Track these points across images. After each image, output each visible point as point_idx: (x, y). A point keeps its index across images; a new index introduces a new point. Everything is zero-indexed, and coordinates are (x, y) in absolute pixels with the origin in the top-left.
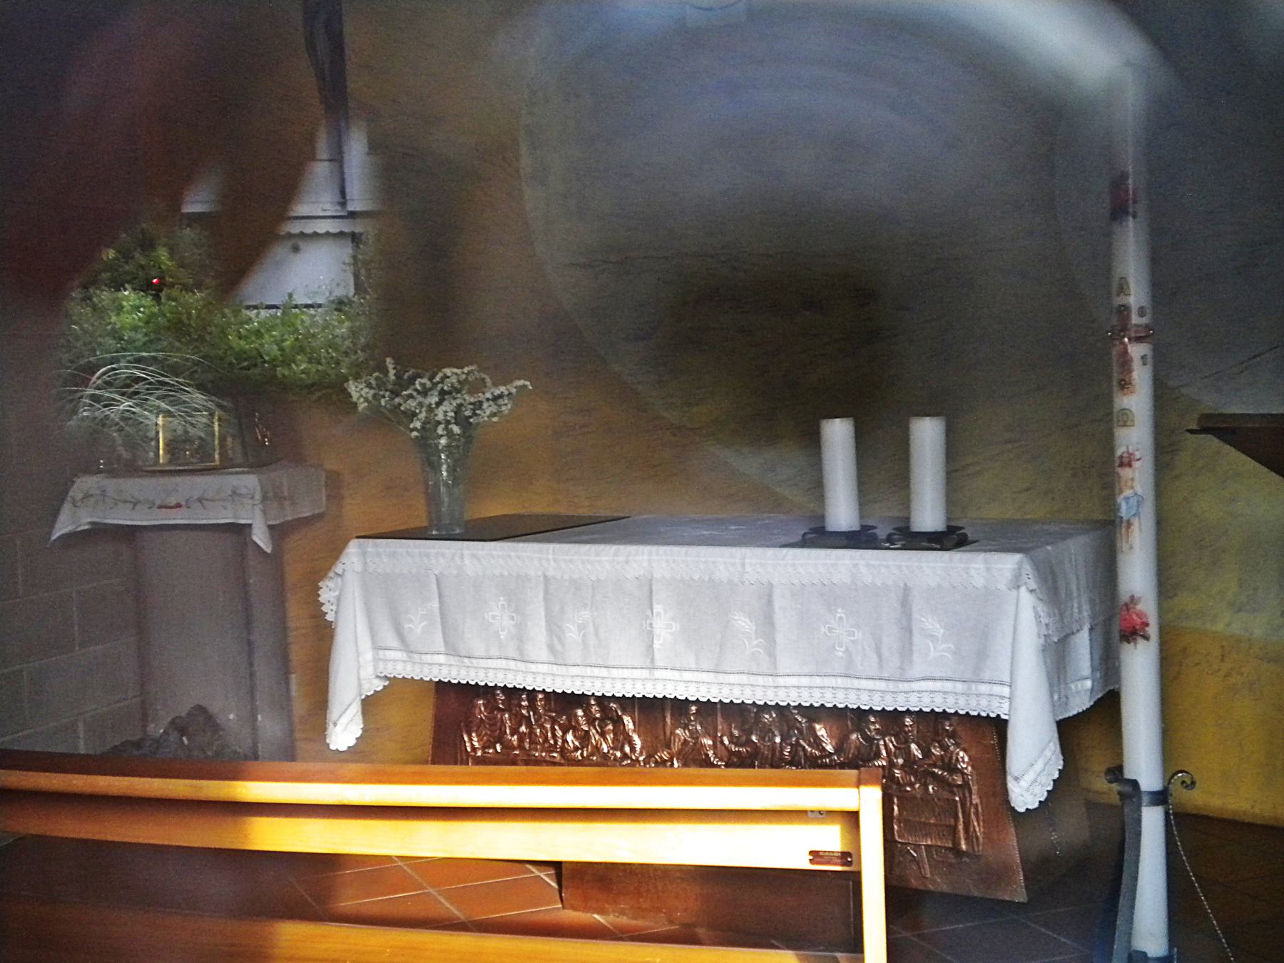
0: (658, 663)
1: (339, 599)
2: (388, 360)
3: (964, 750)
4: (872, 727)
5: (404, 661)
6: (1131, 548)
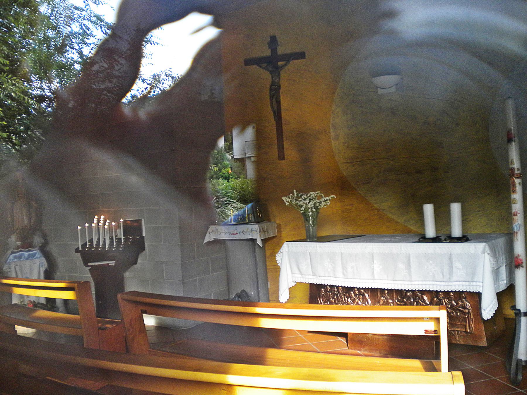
0: (376, 277)
1: (281, 259)
2: (294, 191)
3: (469, 302)
4: (441, 296)
5: (301, 277)
6: (518, 240)
